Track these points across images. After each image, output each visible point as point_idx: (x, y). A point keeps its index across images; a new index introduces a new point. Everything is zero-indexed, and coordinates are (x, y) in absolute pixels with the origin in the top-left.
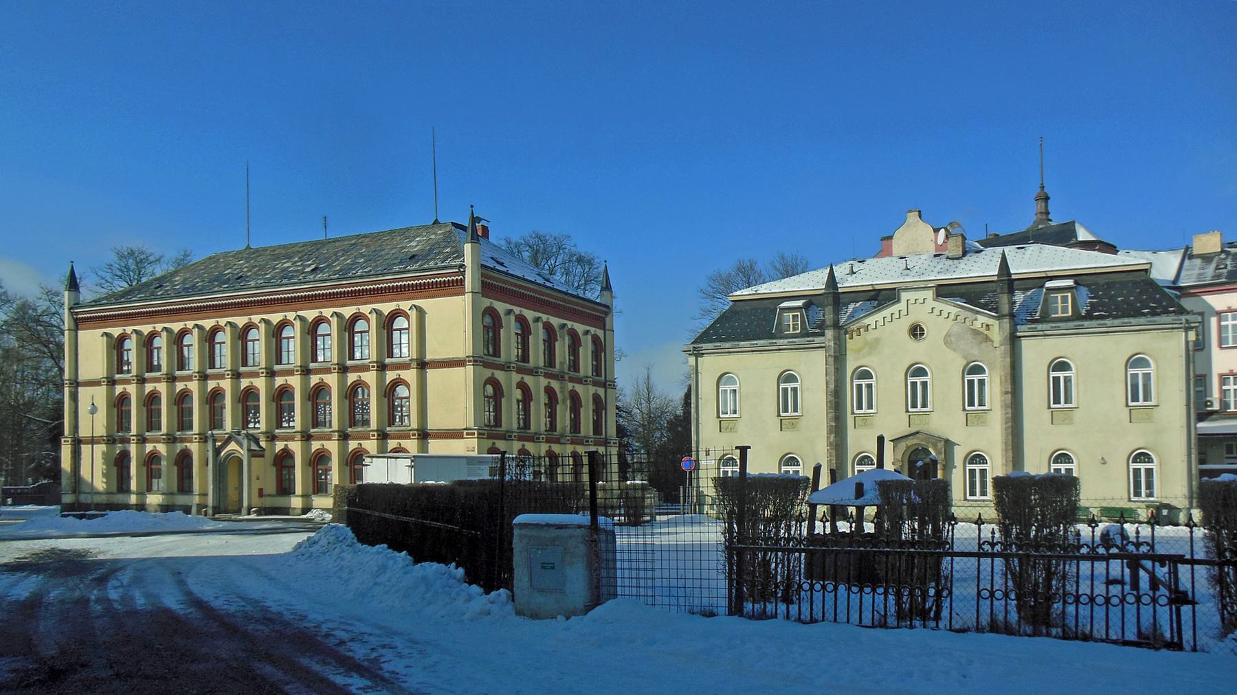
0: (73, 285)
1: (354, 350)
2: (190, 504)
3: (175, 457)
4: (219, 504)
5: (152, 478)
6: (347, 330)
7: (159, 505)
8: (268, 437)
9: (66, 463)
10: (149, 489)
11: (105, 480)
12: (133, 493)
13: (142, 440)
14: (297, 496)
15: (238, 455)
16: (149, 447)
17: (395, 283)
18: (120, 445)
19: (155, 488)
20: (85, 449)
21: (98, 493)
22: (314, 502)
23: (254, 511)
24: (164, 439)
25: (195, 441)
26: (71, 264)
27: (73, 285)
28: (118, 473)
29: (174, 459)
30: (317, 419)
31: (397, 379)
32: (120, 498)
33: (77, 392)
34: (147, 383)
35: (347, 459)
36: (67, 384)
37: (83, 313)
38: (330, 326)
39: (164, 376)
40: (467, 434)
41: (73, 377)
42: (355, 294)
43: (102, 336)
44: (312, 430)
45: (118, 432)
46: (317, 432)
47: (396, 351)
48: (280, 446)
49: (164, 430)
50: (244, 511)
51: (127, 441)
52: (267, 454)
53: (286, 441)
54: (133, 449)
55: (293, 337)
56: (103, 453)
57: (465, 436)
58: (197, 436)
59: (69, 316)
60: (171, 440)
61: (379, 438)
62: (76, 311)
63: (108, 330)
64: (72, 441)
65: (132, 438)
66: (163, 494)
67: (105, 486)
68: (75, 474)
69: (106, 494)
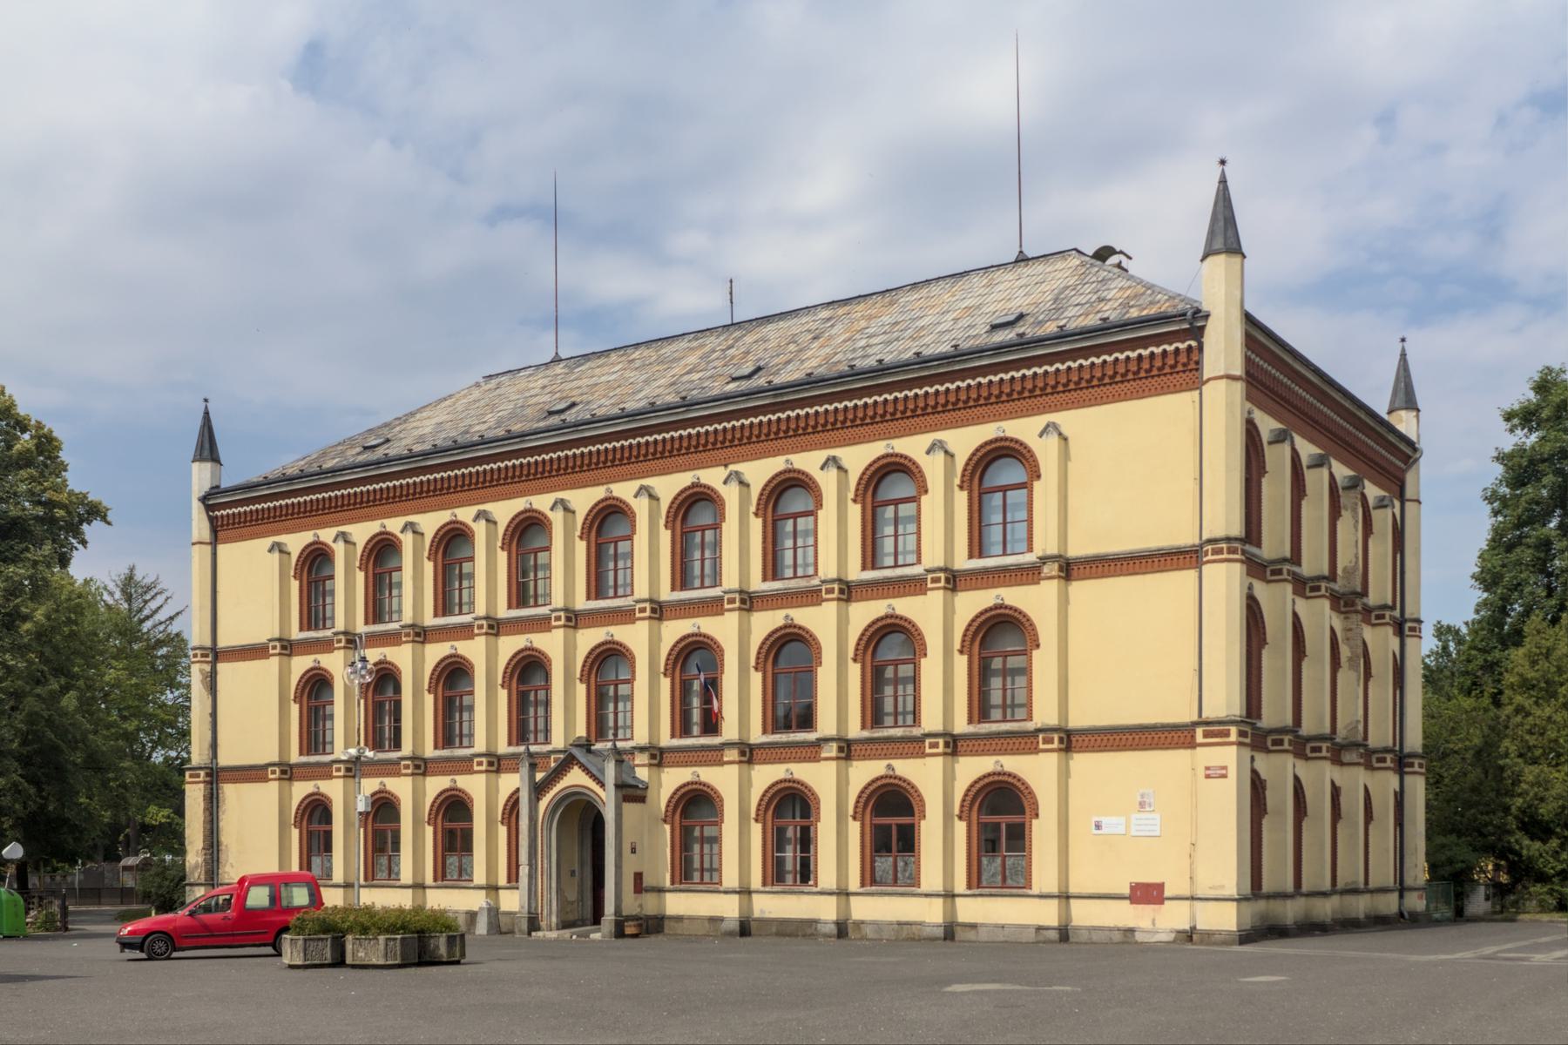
25: (404, 771)
40: (1206, 735)
57: (1199, 738)
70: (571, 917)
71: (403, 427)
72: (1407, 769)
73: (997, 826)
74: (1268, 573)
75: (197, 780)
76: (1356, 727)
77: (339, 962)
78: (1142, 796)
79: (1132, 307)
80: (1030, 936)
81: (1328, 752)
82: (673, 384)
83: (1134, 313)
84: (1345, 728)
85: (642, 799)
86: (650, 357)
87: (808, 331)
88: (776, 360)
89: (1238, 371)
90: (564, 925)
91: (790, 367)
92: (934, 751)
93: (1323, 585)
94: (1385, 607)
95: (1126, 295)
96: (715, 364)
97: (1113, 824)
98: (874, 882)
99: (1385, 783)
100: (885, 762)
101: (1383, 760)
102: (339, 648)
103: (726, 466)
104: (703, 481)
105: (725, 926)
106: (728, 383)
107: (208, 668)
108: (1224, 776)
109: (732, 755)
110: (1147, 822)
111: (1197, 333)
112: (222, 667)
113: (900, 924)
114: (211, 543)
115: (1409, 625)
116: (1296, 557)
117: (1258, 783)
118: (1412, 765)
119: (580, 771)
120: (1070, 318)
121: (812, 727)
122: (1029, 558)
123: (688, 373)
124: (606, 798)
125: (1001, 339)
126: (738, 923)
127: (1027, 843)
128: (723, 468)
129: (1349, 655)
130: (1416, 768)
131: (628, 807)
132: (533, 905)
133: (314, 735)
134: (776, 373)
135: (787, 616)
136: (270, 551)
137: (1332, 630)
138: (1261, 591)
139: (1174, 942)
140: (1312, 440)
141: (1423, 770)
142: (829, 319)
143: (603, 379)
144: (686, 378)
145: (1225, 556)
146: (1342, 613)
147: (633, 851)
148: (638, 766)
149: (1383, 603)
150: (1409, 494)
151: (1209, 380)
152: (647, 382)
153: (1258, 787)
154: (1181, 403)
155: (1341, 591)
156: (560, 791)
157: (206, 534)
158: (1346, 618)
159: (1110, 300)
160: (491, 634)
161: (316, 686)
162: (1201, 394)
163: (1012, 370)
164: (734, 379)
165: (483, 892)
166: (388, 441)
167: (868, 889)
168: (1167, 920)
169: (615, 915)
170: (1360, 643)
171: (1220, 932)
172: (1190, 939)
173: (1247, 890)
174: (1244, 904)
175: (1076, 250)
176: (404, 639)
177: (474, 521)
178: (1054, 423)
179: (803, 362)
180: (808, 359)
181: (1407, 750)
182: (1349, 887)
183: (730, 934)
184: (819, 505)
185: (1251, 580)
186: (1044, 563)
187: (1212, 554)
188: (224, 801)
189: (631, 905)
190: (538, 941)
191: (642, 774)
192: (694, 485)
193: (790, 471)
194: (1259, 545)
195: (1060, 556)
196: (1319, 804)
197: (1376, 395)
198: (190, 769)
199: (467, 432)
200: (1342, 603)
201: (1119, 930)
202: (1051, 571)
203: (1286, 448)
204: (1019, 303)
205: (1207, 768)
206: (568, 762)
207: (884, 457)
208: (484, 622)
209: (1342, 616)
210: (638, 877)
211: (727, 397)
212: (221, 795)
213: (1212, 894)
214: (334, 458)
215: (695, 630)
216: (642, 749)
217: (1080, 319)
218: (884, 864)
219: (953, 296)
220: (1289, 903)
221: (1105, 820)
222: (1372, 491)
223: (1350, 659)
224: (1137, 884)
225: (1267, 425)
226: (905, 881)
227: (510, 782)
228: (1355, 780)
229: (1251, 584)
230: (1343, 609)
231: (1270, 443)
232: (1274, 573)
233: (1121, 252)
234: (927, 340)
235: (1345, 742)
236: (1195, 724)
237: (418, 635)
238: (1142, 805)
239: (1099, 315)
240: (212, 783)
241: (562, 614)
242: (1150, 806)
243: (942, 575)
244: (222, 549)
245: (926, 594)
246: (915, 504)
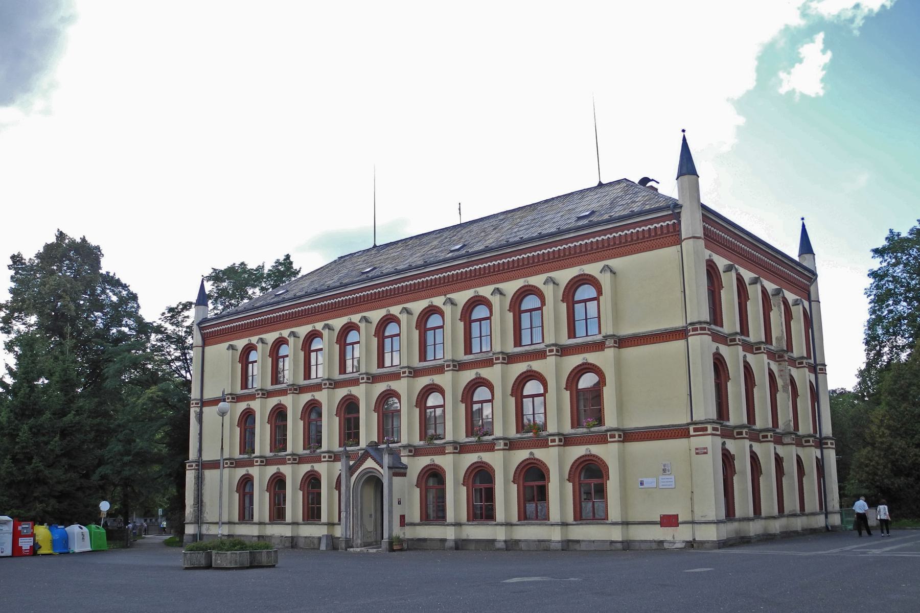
5: (68, 553)
25: (288, 462)
38: (359, 334)
40: (695, 430)
55: (358, 342)
57: (692, 433)
58: (289, 457)
65: (255, 459)
70: (370, 540)
71: (296, 284)
72: (824, 446)
73: (590, 484)
74: (729, 341)
75: (192, 468)
76: (789, 424)
77: (209, 566)
79: (647, 205)
80: (607, 547)
81: (813, 442)
82: (423, 255)
83: (647, 207)
84: (783, 424)
85: (404, 475)
86: (416, 243)
87: (492, 226)
88: (474, 241)
89: (700, 233)
90: (366, 545)
91: (479, 244)
92: (553, 444)
93: (762, 346)
94: (803, 358)
95: (645, 199)
96: (445, 244)
97: (649, 482)
98: (526, 518)
99: (810, 455)
100: (529, 451)
101: (808, 441)
102: (258, 398)
103: (445, 295)
104: (434, 304)
105: (448, 544)
106: (448, 253)
107: (198, 410)
108: (706, 453)
109: (449, 449)
110: (667, 480)
111: (678, 216)
112: (205, 409)
113: (539, 541)
114: (201, 346)
115: (819, 367)
116: (769, 340)
117: (779, 459)
118: (827, 444)
119: (371, 459)
120: (616, 212)
122: (599, 337)
123: (431, 250)
124: (384, 473)
125: (581, 224)
126: (454, 543)
127: (605, 495)
128: (444, 296)
129: (783, 384)
130: (829, 445)
131: (396, 480)
132: (348, 534)
133: (247, 444)
134: (473, 247)
135: (477, 373)
136: (227, 349)
137: (810, 382)
138: (751, 358)
139: (685, 548)
140: (750, 270)
141: (834, 446)
142: (503, 220)
143: (392, 255)
144: (430, 252)
145: (699, 332)
146: (778, 361)
147: (399, 503)
148: (402, 456)
149: (801, 356)
150: (813, 298)
151: (685, 239)
152: (411, 255)
153: (728, 459)
154: (670, 252)
155: (775, 350)
156: (362, 471)
157: (200, 342)
158: (780, 364)
159: (637, 202)
161: (248, 417)
162: (681, 247)
163: (585, 239)
164: (452, 251)
165: (326, 527)
166: (287, 291)
167: (579, 522)
168: (681, 534)
169: (389, 539)
170: (788, 378)
173: (722, 515)
174: (722, 525)
175: (625, 179)
176: (289, 392)
177: (323, 329)
178: (607, 265)
179: (486, 241)
180: (489, 239)
181: (824, 435)
182: (791, 513)
183: (451, 548)
185: (745, 353)
186: (606, 339)
187: (692, 331)
188: (204, 480)
189: (397, 531)
190: (351, 553)
191: (404, 460)
192: (429, 306)
193: (477, 296)
194: (722, 326)
195: (614, 335)
196: (791, 467)
197: (792, 250)
198: (188, 462)
199: (323, 285)
200: (777, 356)
201: (655, 541)
203: (733, 274)
204: (594, 206)
205: (697, 449)
206: (366, 455)
207: (523, 287)
208: (327, 382)
209: (777, 363)
210: (402, 517)
211: (445, 261)
212: (203, 476)
213: (703, 519)
214: (261, 301)
215: (431, 382)
216: (404, 447)
217: (621, 212)
218: (531, 507)
219: (563, 204)
220: (751, 523)
221: (645, 480)
222: (790, 297)
223: (783, 387)
224: (664, 515)
225: (721, 262)
226: (542, 517)
227: (339, 467)
228: (789, 453)
229: (718, 347)
230: (777, 359)
231: (724, 272)
232: (731, 340)
233: (653, 180)
234: (546, 227)
235: (784, 432)
236: (689, 424)
237: (296, 390)
238: (664, 471)
239: (630, 210)
240: (198, 470)
241: (365, 376)
242: (669, 471)
243: (554, 348)
244: (207, 349)
246: (540, 311)
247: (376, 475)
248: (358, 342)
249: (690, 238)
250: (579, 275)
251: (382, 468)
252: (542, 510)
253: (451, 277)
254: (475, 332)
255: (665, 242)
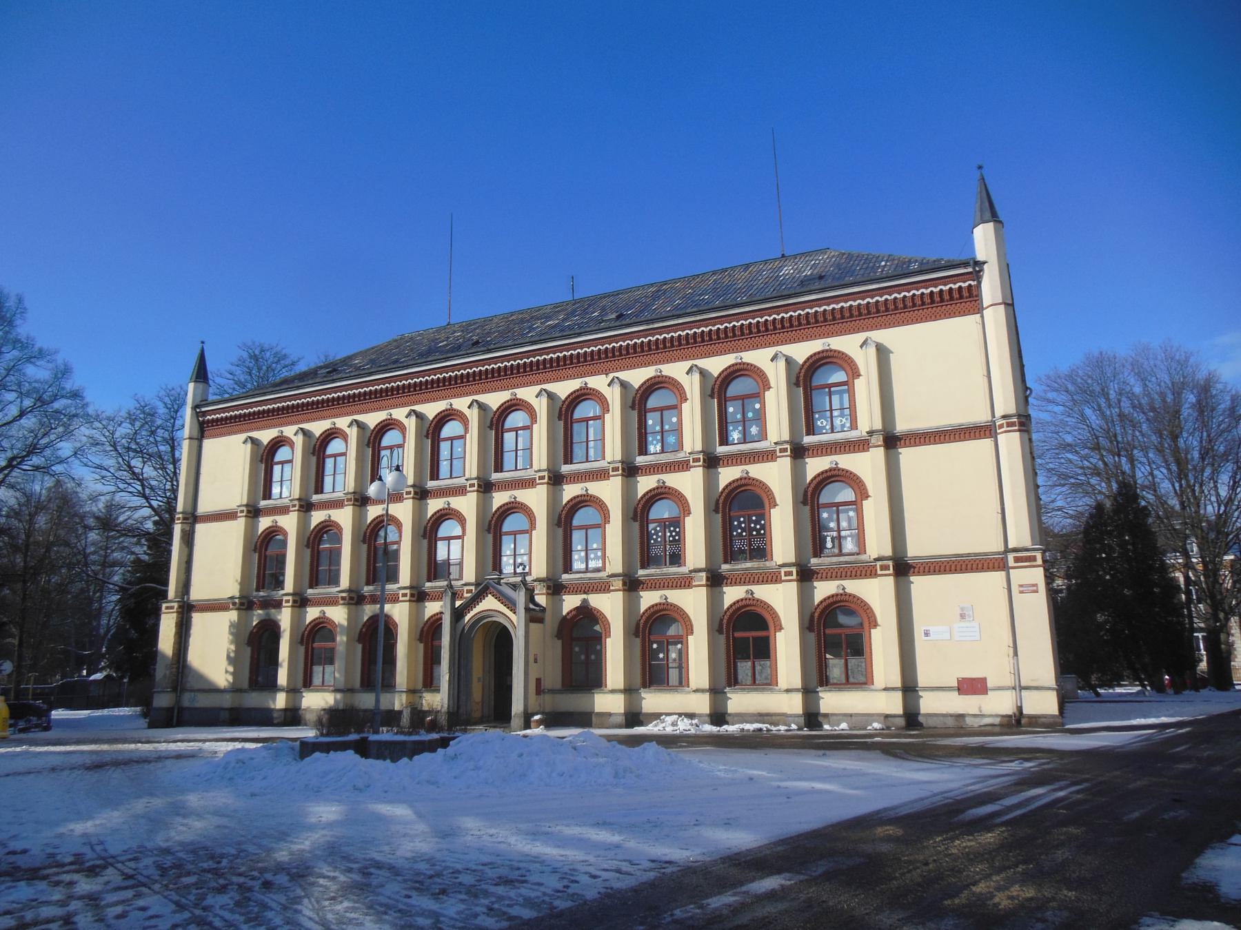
0: (201, 374)
1: (726, 428)
2: (589, 711)
3: (360, 626)
4: (458, 708)
6: (371, 445)
7: (324, 710)
8: (548, 588)
9: (166, 642)
10: (308, 683)
11: (231, 669)
12: (282, 690)
13: (301, 602)
14: (613, 691)
15: (501, 620)
16: (312, 613)
17: (548, 354)
18: (260, 612)
19: (317, 680)
20: (199, 620)
21: (216, 690)
22: (644, 701)
23: (537, 721)
24: (343, 598)
26: (977, 174)
27: (201, 374)
28: (252, 657)
29: (358, 631)
30: (648, 552)
31: (325, 521)
32: (254, 700)
33: (193, 532)
34: (315, 510)
35: (721, 620)
36: (179, 519)
37: (214, 412)
38: (293, 451)
39: (349, 496)
40: (1017, 560)
41: (189, 509)
42: (398, 391)
43: (245, 442)
44: (641, 572)
45: (258, 590)
46: (652, 575)
47: (276, 490)
48: (570, 602)
49: (345, 581)
50: (516, 721)
51: (278, 605)
52: (548, 616)
53: (585, 593)
54: (285, 618)
56: (232, 625)
57: (1011, 563)
59: (191, 418)
60: (355, 599)
61: (550, 592)
62: (203, 409)
63: (255, 434)
64: (180, 607)
65: (285, 598)
66: (336, 691)
67: (230, 678)
68: (179, 658)
69: (234, 691)
78: (962, 609)
121: (556, 636)
131: (533, 626)
147: (536, 661)
154: (972, 320)
160: (352, 604)
163: (833, 303)
168: (999, 704)
171: (1045, 716)
172: (1018, 722)
184: (684, 398)
201: (951, 715)
202: (878, 441)
210: (538, 681)
221: (932, 629)
238: (962, 616)
245: (328, 753)
247: (494, 619)
248: (290, 461)
249: (992, 305)
250: (823, 351)
251: (515, 613)
252: (761, 672)
253: (502, 370)
254: (579, 435)
255: (762, 342)
